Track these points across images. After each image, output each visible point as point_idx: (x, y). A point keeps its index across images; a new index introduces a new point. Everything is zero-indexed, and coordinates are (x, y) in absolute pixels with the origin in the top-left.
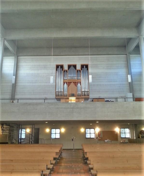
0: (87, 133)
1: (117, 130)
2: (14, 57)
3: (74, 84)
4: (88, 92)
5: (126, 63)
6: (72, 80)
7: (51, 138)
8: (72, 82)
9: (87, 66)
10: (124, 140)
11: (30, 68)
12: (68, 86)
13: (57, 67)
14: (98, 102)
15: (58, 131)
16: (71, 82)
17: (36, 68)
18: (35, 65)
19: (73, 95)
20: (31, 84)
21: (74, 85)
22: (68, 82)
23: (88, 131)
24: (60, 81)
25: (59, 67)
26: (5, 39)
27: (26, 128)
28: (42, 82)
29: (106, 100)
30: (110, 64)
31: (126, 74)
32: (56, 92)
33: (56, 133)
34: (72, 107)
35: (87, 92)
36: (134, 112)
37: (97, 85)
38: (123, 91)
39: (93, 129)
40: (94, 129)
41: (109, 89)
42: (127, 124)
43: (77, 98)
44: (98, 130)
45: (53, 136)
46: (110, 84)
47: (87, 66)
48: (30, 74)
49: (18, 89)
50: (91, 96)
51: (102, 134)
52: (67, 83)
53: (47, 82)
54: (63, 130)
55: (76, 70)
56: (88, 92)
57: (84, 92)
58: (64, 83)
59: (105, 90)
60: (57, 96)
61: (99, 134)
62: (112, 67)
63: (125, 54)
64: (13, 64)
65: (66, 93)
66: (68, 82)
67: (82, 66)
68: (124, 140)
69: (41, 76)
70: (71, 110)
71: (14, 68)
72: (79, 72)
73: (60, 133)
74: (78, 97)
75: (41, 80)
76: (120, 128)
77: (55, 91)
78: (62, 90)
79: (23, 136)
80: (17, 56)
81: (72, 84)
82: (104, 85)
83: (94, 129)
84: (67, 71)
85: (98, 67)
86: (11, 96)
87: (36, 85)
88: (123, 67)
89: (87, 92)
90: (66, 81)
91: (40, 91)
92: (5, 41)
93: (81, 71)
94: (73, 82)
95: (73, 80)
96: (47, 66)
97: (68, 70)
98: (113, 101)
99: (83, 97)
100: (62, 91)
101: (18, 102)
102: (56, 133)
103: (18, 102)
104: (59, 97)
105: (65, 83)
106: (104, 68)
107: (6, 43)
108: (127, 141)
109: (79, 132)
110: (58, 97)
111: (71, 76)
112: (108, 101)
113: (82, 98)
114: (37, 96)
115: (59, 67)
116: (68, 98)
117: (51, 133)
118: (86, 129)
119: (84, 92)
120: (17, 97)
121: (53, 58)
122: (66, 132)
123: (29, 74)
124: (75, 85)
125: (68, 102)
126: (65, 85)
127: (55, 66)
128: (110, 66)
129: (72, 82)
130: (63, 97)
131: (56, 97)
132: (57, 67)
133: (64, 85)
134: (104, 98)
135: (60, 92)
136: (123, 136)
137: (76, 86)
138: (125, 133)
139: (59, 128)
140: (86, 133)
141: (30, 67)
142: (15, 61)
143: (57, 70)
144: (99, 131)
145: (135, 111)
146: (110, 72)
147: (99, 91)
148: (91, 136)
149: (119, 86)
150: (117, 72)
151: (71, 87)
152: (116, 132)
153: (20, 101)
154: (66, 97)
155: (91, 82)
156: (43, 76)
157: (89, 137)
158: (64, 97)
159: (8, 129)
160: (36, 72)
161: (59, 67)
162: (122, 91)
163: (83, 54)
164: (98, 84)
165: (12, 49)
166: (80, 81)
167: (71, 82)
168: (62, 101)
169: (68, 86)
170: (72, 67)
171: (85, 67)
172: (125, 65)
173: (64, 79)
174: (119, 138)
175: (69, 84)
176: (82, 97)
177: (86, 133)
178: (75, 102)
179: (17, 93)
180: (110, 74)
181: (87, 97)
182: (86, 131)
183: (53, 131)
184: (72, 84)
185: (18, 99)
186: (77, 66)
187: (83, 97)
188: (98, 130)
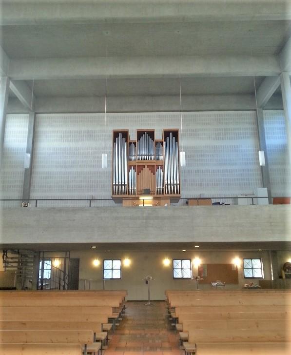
0: (176, 268)
1: (236, 261)
2: (28, 115)
3: (150, 170)
4: (178, 186)
5: (255, 126)
6: (146, 161)
7: (103, 278)
8: (146, 166)
9: (175, 134)
10: (251, 281)
11: (61, 137)
12: (138, 174)
13: (116, 134)
14: (198, 207)
15: (117, 264)
16: (144, 166)
17: (72, 137)
18: (70, 131)
19: (147, 192)
20: (63, 170)
21: (150, 171)
22: (138, 166)
23: (178, 263)
24: (122, 164)
25: (120, 136)
26: (10, 78)
27: (52, 258)
28: (84, 165)
29: (214, 201)
30: (222, 129)
31: (255, 149)
32: (113, 185)
33: (112, 269)
34: (145, 215)
35: (175, 186)
36: (271, 226)
37: (196, 171)
38: (249, 183)
39: (189, 261)
40: (191, 260)
41: (221, 179)
42: (256, 250)
43: (155, 198)
44: (198, 262)
45: (107, 275)
46: (222, 170)
47: (175, 134)
48: (61, 148)
49: (37, 180)
50: (185, 194)
51: (206, 270)
52: (135, 167)
53: (96, 165)
54: (127, 262)
55: (154, 141)
56: (178, 186)
57: (169, 187)
58: (130, 167)
59: (212, 181)
60: (115, 194)
61: (200, 271)
62: (226, 136)
63: (253, 108)
64: (27, 129)
65: (133, 187)
66: (137, 164)
67: (166, 134)
68: (251, 281)
69: (83, 153)
70: (144, 221)
71: (29, 137)
72: (159, 145)
73: (122, 269)
74: (158, 196)
75: (83, 162)
76: (243, 259)
77: (112, 184)
78: (126, 181)
79: (47, 275)
80: (34, 113)
81: (146, 169)
82: (209, 172)
83: (191, 260)
84: (135, 143)
85: (198, 135)
86: (22, 194)
87: (73, 172)
88: (249, 136)
89: (175, 186)
90: (133, 163)
91: (80, 184)
92: (11, 83)
93: (164, 143)
94: (148, 166)
95: (148, 161)
96: (96, 134)
97: (138, 141)
98: (229, 205)
99: (167, 195)
100: (126, 184)
101: (36, 206)
102: (112, 269)
103: (36, 206)
104: (120, 196)
105: (132, 167)
106: (209, 137)
107: (12, 86)
108: (256, 284)
109: (160, 267)
110: (117, 196)
111: (144, 153)
112: (218, 204)
113: (166, 198)
114: (76, 195)
115: (119, 136)
116: (138, 199)
117: (104, 269)
118: (173, 260)
119: (169, 187)
120: (34, 195)
121: (107, 117)
122: (134, 267)
123: (59, 150)
124: (152, 172)
125: (137, 205)
126: (132, 171)
127: (112, 134)
128: (223, 133)
129: (146, 166)
130: (127, 196)
131: (114, 196)
132: (116, 134)
133: (129, 171)
134: (210, 199)
135: (122, 185)
136: (249, 275)
137: (154, 174)
138: (252, 268)
139: (120, 258)
140: (173, 269)
141: (61, 135)
142: (30, 123)
143: (115, 141)
144: (199, 265)
145: (272, 224)
146: (223, 146)
147: (201, 184)
148: (184, 274)
149: (241, 174)
150: (237, 146)
151: (144, 175)
152: (235, 265)
153: (40, 203)
154: (134, 196)
155: (183, 165)
156: (87, 154)
157: (180, 277)
158: (130, 196)
159: (17, 260)
160: (72, 145)
161: (120, 136)
162: (247, 183)
163: (167, 109)
164: (198, 170)
165: (24, 99)
166: (162, 164)
167: (144, 166)
168: (126, 203)
169: (138, 174)
170: (146, 136)
171: (172, 135)
172: (253, 131)
173: (129, 160)
174: (240, 277)
175: (139, 169)
176: (165, 195)
177: (173, 269)
178: (151, 205)
179: (34, 188)
180: (222, 149)
181: (175, 195)
182: (175, 264)
183: (108, 264)
184: (146, 169)
185: (37, 200)
186: (156, 133)
187: (167, 195)
188: (198, 262)
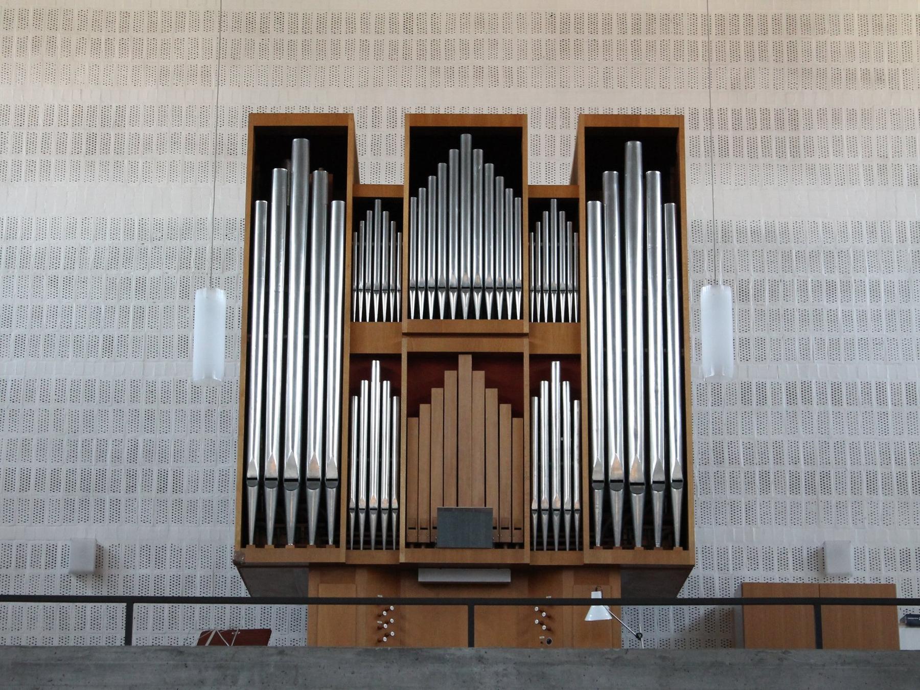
3: (489, 384)
6: (465, 326)
8: (465, 363)
12: (413, 412)
14: (816, 656)
16: (450, 360)
21: (493, 393)
22: (410, 355)
32: (245, 481)
41: (778, 445)
53: (49, 339)
55: (518, 193)
60: (260, 541)
66: (405, 348)
69: (41, 255)
72: (554, 218)
75: (37, 313)
77: (233, 465)
82: (882, 401)
84: (393, 206)
85: (810, 152)
87: (60, 383)
91: (19, 465)
94: (480, 360)
95: (477, 326)
96: (128, 130)
97: (413, 193)
100: (332, 473)
104: (290, 554)
106: (883, 169)
110: (270, 554)
115: (289, 157)
124: (502, 400)
129: (465, 363)
130: (339, 555)
133: (355, 390)
135: (303, 482)
137: (517, 413)
147: (825, 476)
154: (382, 557)
156: (70, 266)
157: (745, 607)
158: (363, 557)
164: (806, 387)
166: (568, 350)
169: (413, 412)
176: (589, 556)
181: (659, 557)
186: (532, 134)
187: (606, 557)
